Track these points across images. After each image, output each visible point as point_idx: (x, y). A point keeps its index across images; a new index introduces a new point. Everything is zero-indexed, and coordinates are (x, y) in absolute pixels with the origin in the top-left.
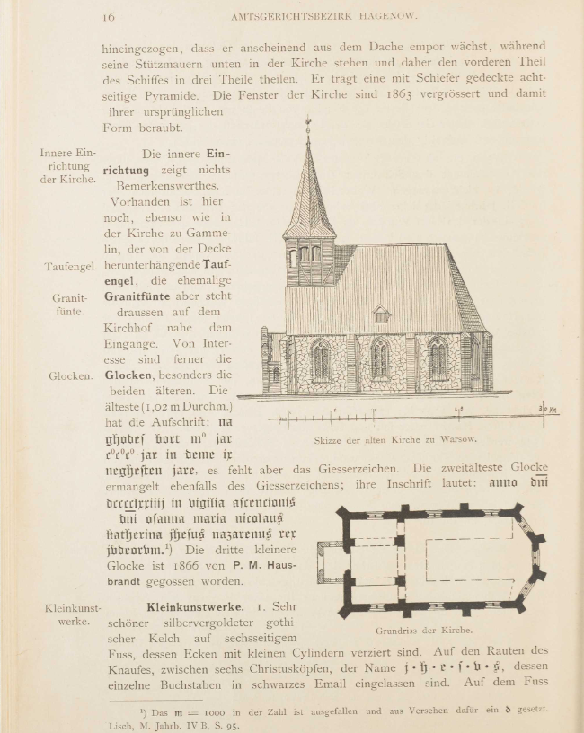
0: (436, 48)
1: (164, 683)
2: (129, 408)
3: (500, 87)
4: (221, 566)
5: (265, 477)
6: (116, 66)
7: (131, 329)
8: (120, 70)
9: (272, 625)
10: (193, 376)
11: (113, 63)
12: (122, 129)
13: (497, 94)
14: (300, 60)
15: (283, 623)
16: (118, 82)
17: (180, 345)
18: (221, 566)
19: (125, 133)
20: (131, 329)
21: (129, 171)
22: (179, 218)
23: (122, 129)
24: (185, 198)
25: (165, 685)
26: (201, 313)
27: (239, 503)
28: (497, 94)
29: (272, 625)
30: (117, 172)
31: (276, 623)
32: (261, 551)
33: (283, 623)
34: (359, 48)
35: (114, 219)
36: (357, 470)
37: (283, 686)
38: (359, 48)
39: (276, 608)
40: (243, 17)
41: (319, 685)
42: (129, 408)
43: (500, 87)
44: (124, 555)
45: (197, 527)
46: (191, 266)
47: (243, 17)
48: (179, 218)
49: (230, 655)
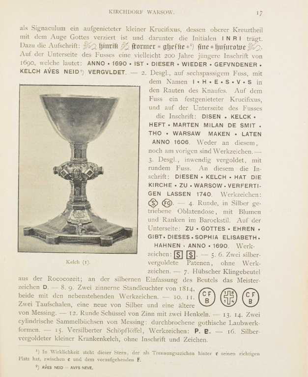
0: (154, 151)
3: (175, 336)
5: (153, 326)
9: (31, 339)
13: (174, 340)
22: (180, 211)
24: (124, 36)
25: (175, 281)
26: (230, 109)
27: (223, 47)
28: (174, 340)
29: (31, 339)
30: (176, 332)
32: (129, 30)
35: (154, 151)
37: (104, 29)
39: (109, 331)
40: (137, 12)
41: (148, 280)
43: (175, 336)
44: (140, 49)
46: (203, 212)
47: (137, 12)
48: (180, 211)
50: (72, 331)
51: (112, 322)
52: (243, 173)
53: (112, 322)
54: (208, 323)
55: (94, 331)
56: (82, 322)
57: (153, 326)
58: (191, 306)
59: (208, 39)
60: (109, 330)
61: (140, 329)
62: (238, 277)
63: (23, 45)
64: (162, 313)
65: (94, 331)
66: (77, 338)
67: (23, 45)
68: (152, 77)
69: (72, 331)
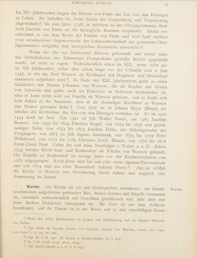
1: (161, 25)
2: (31, 107)
4: (106, 36)
5: (94, 83)
6: (20, 101)
7: (60, 96)
8: (141, 77)
10: (87, 81)
11: (149, 25)
12: (63, 209)
14: (128, 156)
15: (68, 193)
16: (79, 86)
17: (80, 108)
18: (106, 36)
19: (65, 210)
20: (60, 96)
21: (125, 20)
23: (63, 209)
31: (66, 193)
33: (68, 193)
34: (58, 25)
36: (80, 19)
38: (58, 25)
42: (31, 107)
45: (89, 78)
49: (80, 97)
50: (147, 21)
51: (147, 71)
52: (95, 105)
53: (147, 71)
54: (54, 156)
55: (109, 168)
56: (136, 48)
57: (94, 83)
58: (26, 24)
59: (147, 37)
60: (72, 53)
61: (104, 74)
62: (116, 105)
63: (149, 31)
64: (87, 187)
65: (109, 168)
66: (153, 210)
67: (149, 31)
68: (90, 110)
69: (147, 21)
